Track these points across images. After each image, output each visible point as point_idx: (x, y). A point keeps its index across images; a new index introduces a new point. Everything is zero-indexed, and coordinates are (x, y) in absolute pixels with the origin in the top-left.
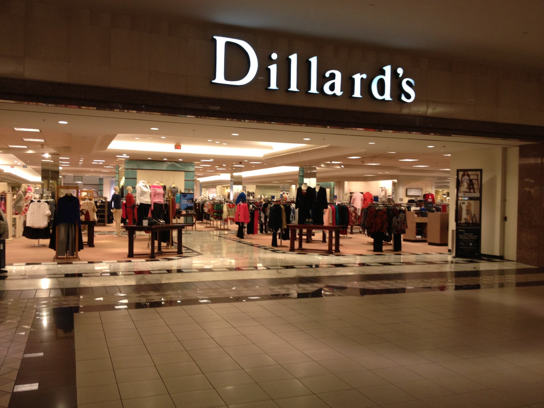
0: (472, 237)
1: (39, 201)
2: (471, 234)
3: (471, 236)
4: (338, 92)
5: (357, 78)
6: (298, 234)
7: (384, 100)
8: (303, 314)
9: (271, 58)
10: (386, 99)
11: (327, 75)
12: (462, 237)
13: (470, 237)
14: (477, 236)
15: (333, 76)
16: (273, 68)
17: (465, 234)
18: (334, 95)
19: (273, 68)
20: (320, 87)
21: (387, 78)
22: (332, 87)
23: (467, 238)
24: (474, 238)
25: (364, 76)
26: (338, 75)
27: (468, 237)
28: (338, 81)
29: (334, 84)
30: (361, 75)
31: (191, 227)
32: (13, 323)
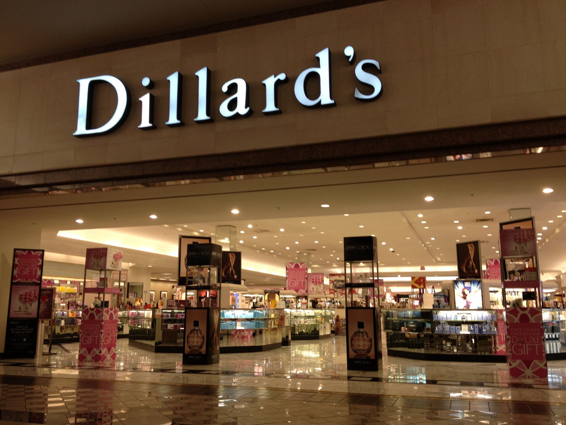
0: (28, 331)
1: (484, 257)
2: (26, 327)
3: (26, 329)
4: (241, 109)
5: (270, 83)
6: (124, 314)
7: (237, 114)
8: (356, 414)
9: (243, 79)
10: (323, 103)
11: (225, 88)
12: (14, 331)
13: (25, 331)
14: (33, 329)
15: (233, 88)
16: (145, 100)
17: (18, 327)
18: (237, 114)
19: (145, 100)
20: (212, 108)
21: (324, 72)
22: (233, 105)
23: (20, 332)
24: (29, 332)
25: (282, 77)
26: (241, 84)
27: (21, 330)
28: (241, 95)
29: (235, 100)
30: (275, 77)
31: (436, 292)
32: (232, 386)
